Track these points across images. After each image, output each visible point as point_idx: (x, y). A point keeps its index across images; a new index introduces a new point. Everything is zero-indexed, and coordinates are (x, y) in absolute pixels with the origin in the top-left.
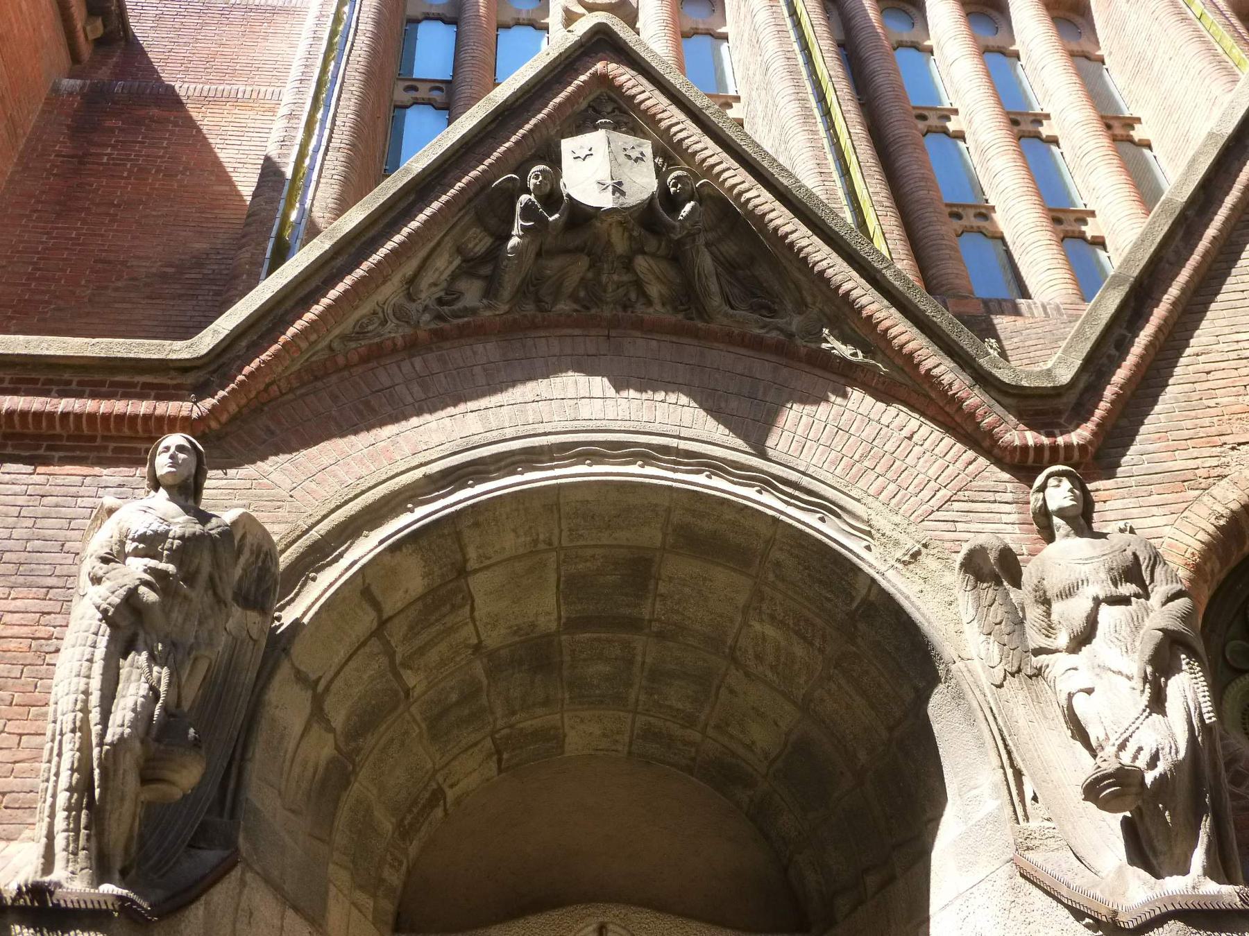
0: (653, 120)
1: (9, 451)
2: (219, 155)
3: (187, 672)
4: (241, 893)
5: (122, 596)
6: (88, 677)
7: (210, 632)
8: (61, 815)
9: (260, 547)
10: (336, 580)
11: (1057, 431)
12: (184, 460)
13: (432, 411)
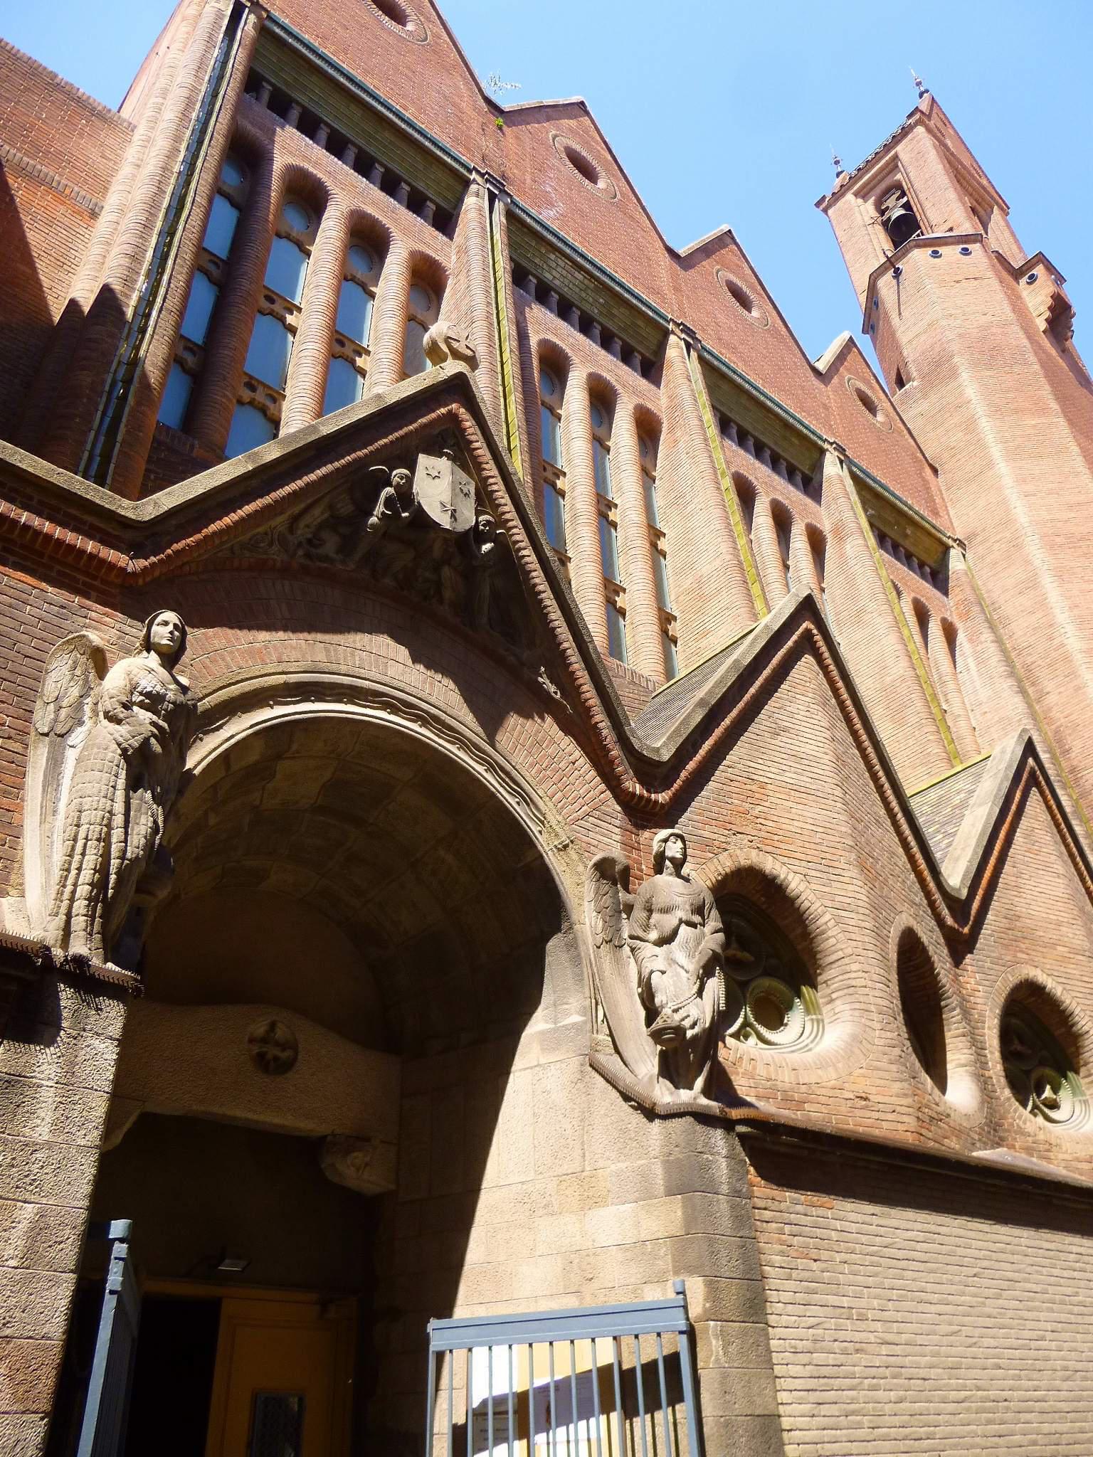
0: (479, 467)
2: (28, 235)
10: (219, 746)
11: (652, 790)
13: (294, 631)
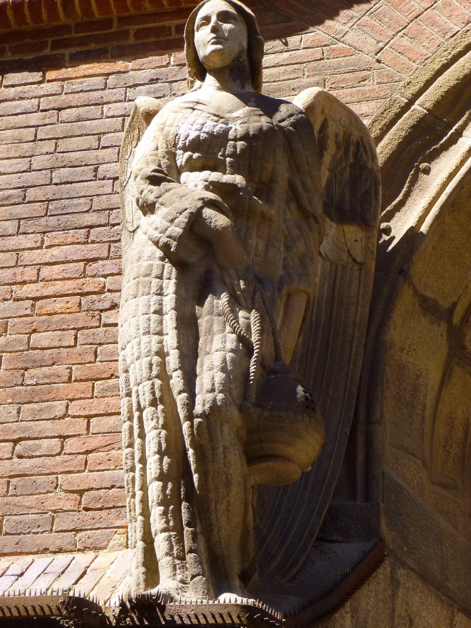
1: (8, 56)
3: (281, 314)
4: (394, 597)
5: (183, 225)
6: (160, 333)
7: (302, 258)
8: (156, 511)
9: (348, 136)
10: (458, 168)
12: (230, 31)
